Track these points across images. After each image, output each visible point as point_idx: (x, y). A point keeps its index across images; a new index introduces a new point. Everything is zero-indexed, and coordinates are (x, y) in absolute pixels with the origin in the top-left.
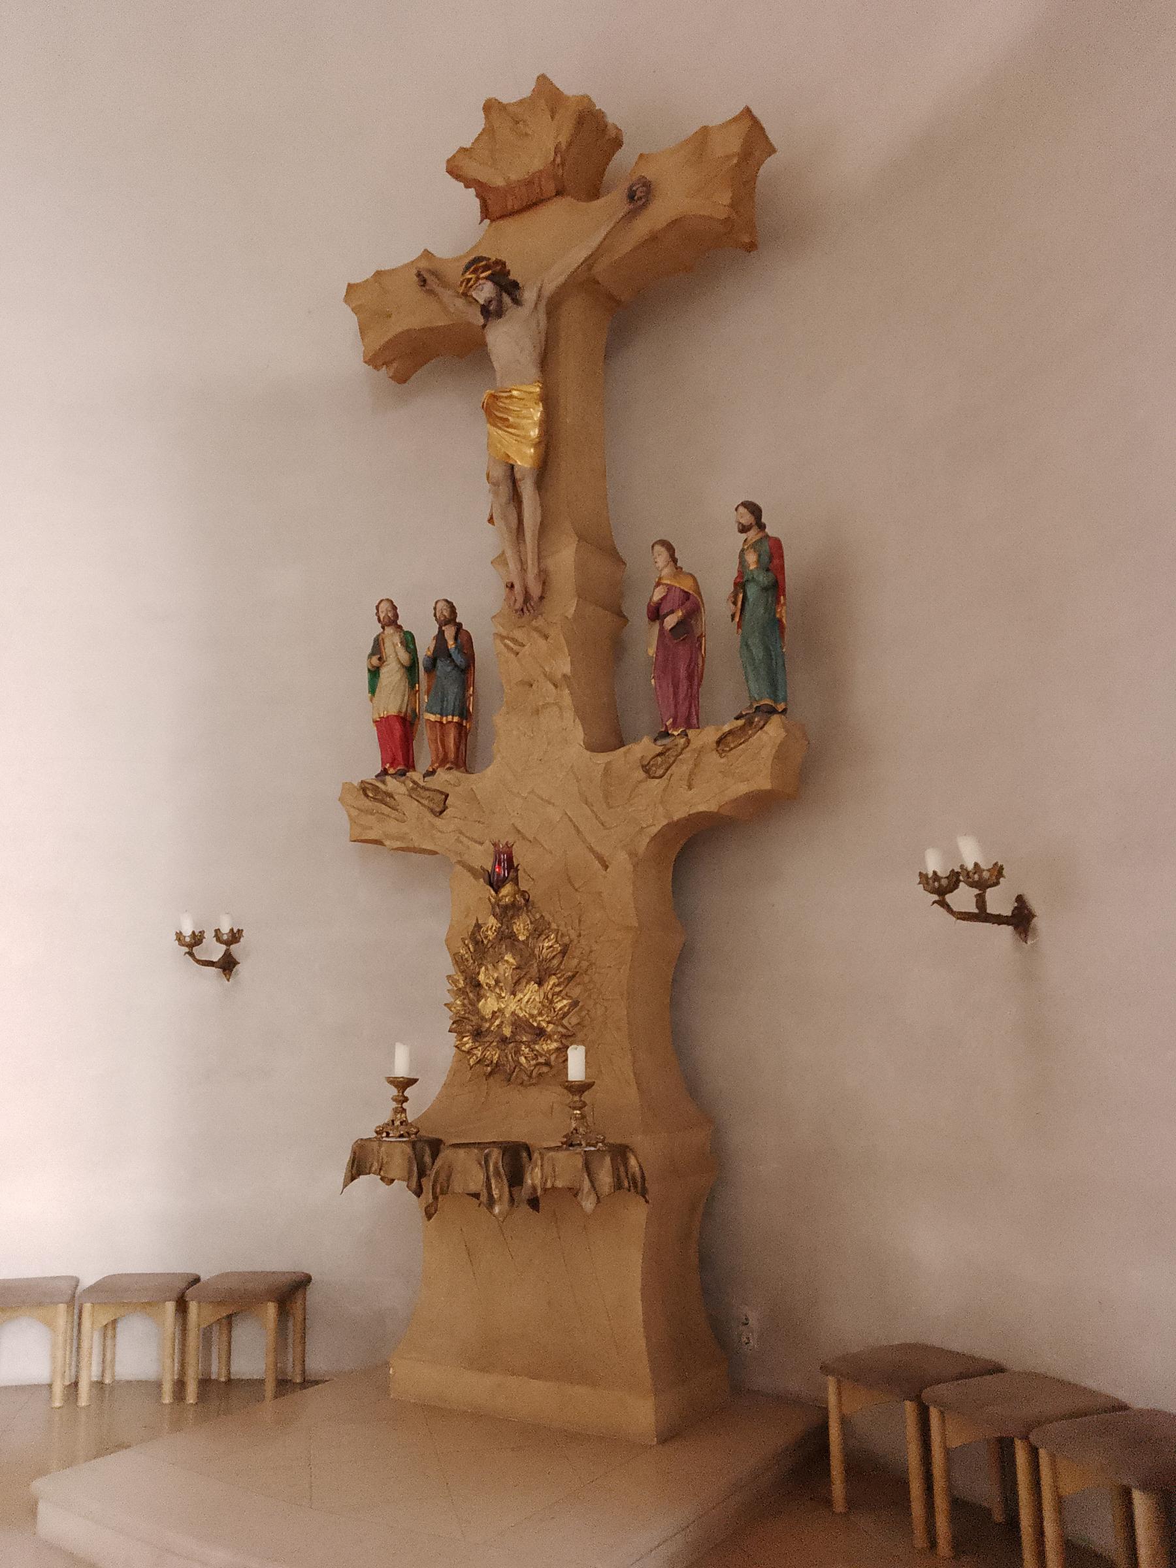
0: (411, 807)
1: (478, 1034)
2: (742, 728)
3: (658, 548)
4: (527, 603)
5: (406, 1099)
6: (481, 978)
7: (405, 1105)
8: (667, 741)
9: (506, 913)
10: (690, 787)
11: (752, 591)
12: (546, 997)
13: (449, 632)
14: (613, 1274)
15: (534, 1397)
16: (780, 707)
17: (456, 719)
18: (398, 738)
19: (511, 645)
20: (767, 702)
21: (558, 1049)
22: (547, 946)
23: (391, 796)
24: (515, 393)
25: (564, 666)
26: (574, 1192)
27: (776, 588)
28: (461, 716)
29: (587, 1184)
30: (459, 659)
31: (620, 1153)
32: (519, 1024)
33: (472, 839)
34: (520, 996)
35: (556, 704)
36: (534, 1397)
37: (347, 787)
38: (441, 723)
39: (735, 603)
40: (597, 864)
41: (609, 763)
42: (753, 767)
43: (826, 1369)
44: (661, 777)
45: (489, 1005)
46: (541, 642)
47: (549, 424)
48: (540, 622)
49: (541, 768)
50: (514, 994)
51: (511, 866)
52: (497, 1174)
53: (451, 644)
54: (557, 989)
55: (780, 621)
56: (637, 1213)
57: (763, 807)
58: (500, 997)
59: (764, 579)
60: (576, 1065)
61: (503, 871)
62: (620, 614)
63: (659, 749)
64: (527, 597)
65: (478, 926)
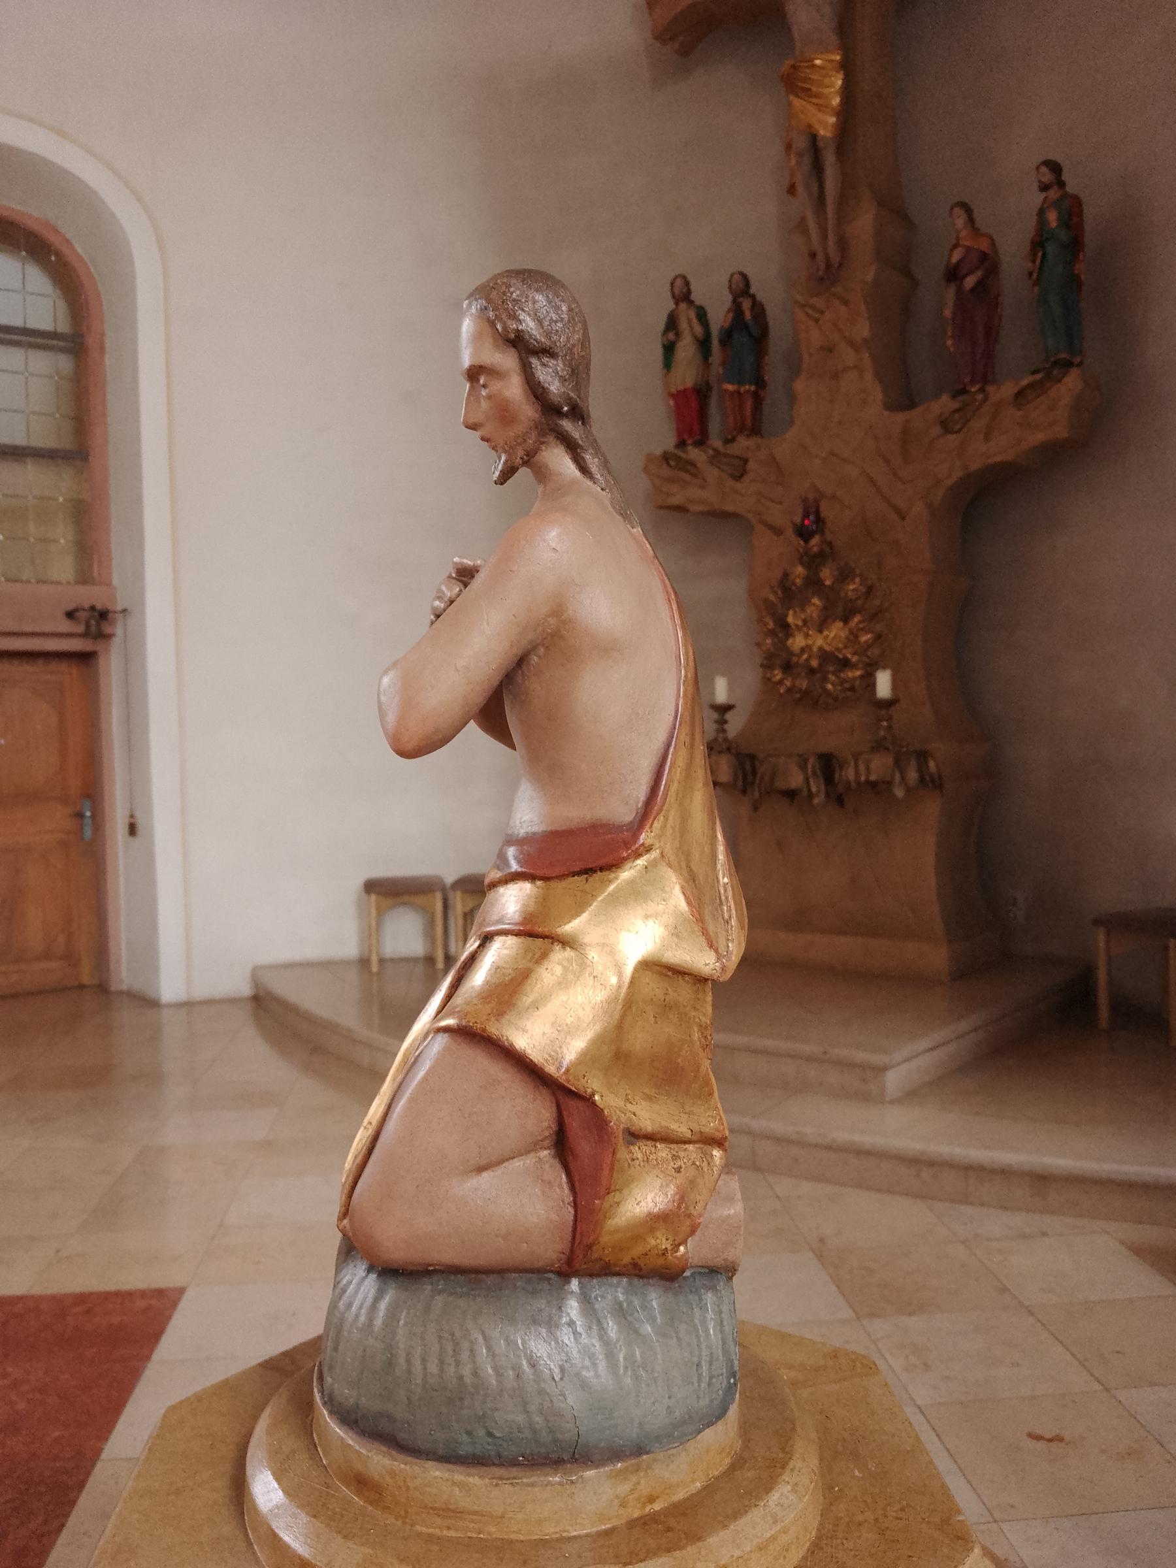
0: (712, 474)
1: (787, 667)
2: (1041, 381)
3: (957, 210)
4: (826, 275)
5: (726, 722)
6: (790, 619)
7: (726, 726)
8: (965, 397)
9: (813, 561)
10: (987, 439)
11: (1051, 248)
12: (851, 632)
13: (746, 304)
14: (911, 856)
15: (847, 948)
16: (1077, 360)
17: (753, 388)
18: (691, 412)
19: (810, 312)
20: (1063, 356)
21: (861, 677)
22: (852, 587)
23: (693, 464)
24: (818, 62)
25: (863, 330)
26: (889, 783)
27: (1075, 245)
28: (757, 385)
29: (898, 777)
30: (756, 331)
31: (922, 756)
32: (825, 657)
33: (771, 500)
34: (826, 633)
35: (855, 367)
36: (847, 948)
37: (650, 459)
38: (738, 392)
39: (1034, 262)
40: (894, 516)
41: (907, 421)
42: (1052, 416)
43: (1097, 922)
44: (959, 431)
45: (798, 642)
46: (843, 308)
47: (848, 93)
48: (838, 289)
49: (838, 429)
50: (821, 632)
51: (819, 520)
52: (814, 773)
53: (748, 315)
54: (861, 626)
55: (1078, 276)
56: (932, 809)
57: (1054, 457)
58: (807, 636)
59: (1064, 235)
60: (884, 684)
61: (811, 523)
62: (907, 272)
63: (957, 405)
64: (829, 266)
65: (786, 575)
